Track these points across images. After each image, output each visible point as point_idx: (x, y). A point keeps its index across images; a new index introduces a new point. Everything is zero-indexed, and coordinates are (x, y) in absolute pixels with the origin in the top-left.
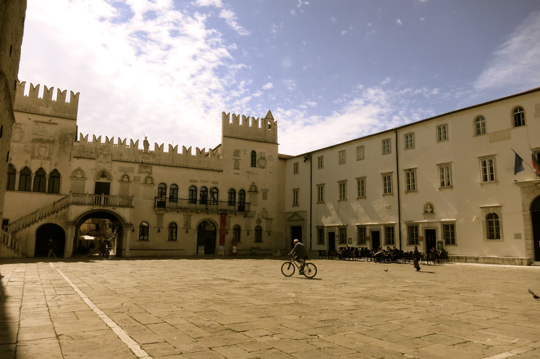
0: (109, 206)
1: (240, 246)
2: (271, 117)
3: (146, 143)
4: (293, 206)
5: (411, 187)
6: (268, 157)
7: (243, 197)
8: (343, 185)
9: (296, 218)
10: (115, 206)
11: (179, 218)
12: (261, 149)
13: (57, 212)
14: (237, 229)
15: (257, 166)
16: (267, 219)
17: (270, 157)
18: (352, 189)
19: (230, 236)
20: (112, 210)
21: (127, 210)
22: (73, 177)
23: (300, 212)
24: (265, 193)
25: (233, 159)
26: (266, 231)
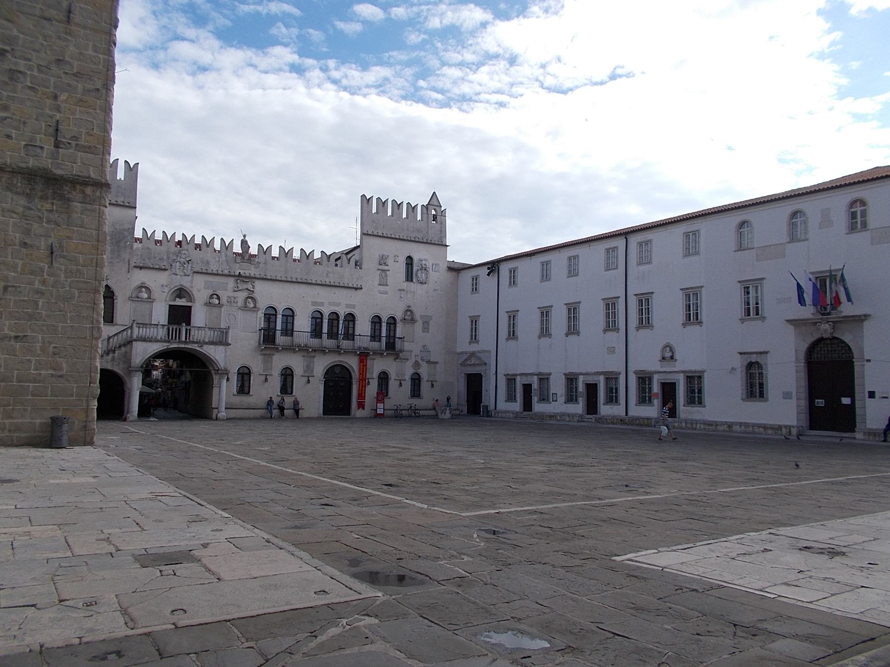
0: (194, 342)
1: (390, 403)
2: (436, 203)
3: (244, 243)
4: (470, 343)
5: (645, 322)
6: (431, 268)
7: (392, 328)
8: (545, 313)
9: (473, 361)
10: (201, 343)
11: (296, 363)
12: (420, 253)
13: (114, 351)
14: (384, 378)
15: (414, 281)
16: (428, 362)
17: (434, 266)
18: (559, 320)
19: (372, 389)
20: (198, 349)
21: (221, 348)
22: (135, 298)
23: (479, 352)
24: (426, 322)
25: (378, 269)
26: (428, 381)
